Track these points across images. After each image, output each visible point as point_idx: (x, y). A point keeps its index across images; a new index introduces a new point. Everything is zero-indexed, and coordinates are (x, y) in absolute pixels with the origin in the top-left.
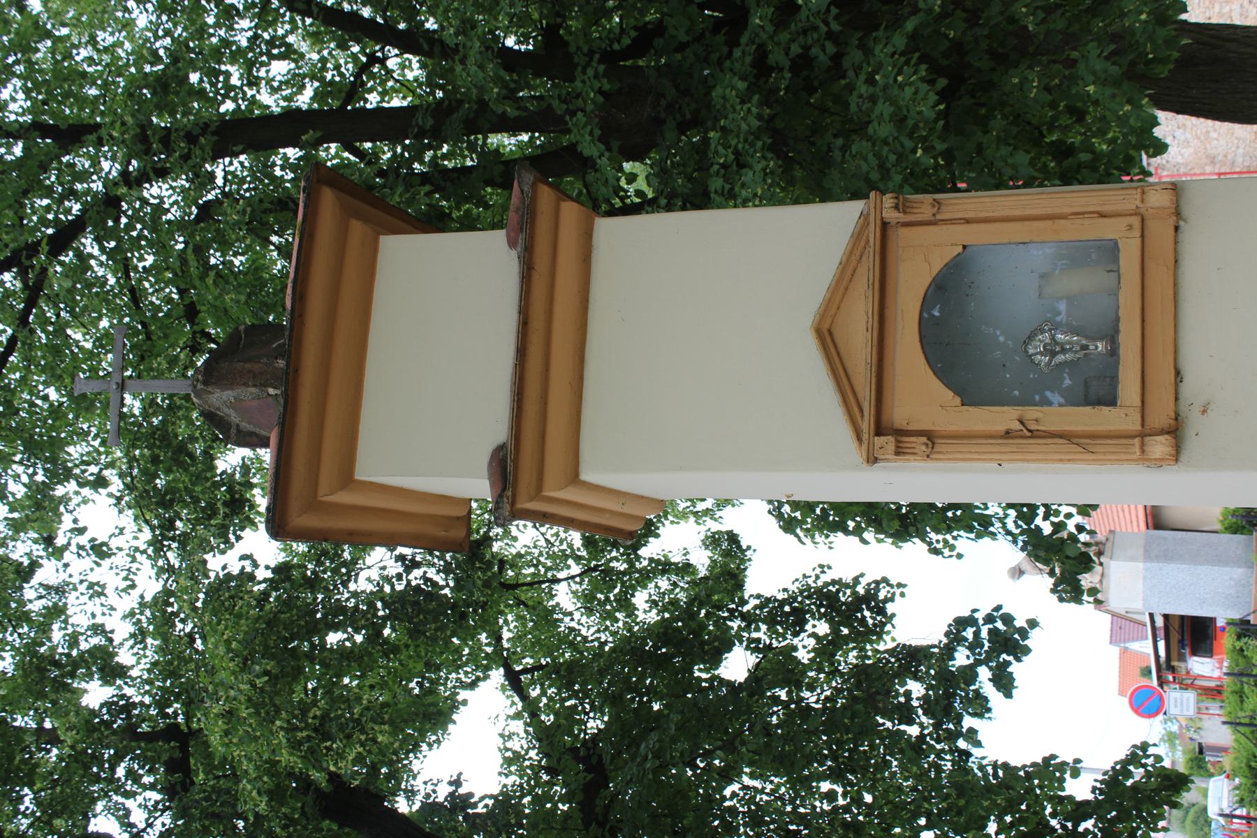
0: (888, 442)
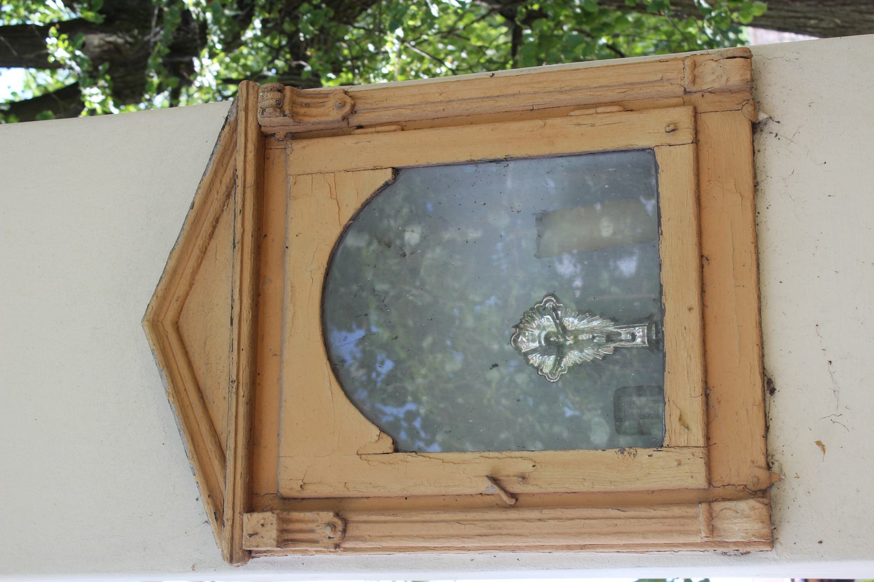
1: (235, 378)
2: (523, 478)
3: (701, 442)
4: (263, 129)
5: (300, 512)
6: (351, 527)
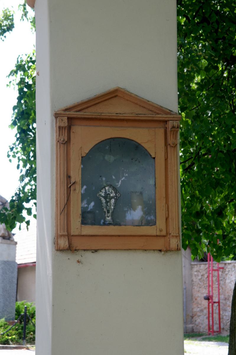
0: (65, 123)
1: (102, 115)
2: (75, 190)
3: (82, 234)
4: (168, 122)
5: (195, 341)
6: (63, 145)
